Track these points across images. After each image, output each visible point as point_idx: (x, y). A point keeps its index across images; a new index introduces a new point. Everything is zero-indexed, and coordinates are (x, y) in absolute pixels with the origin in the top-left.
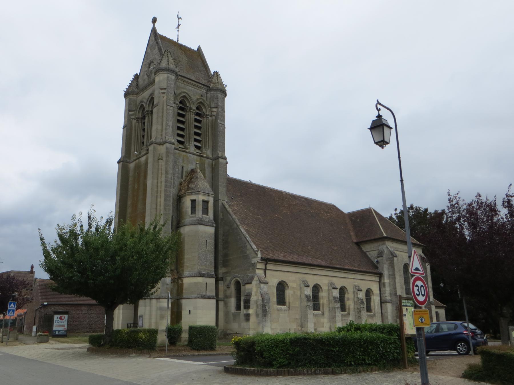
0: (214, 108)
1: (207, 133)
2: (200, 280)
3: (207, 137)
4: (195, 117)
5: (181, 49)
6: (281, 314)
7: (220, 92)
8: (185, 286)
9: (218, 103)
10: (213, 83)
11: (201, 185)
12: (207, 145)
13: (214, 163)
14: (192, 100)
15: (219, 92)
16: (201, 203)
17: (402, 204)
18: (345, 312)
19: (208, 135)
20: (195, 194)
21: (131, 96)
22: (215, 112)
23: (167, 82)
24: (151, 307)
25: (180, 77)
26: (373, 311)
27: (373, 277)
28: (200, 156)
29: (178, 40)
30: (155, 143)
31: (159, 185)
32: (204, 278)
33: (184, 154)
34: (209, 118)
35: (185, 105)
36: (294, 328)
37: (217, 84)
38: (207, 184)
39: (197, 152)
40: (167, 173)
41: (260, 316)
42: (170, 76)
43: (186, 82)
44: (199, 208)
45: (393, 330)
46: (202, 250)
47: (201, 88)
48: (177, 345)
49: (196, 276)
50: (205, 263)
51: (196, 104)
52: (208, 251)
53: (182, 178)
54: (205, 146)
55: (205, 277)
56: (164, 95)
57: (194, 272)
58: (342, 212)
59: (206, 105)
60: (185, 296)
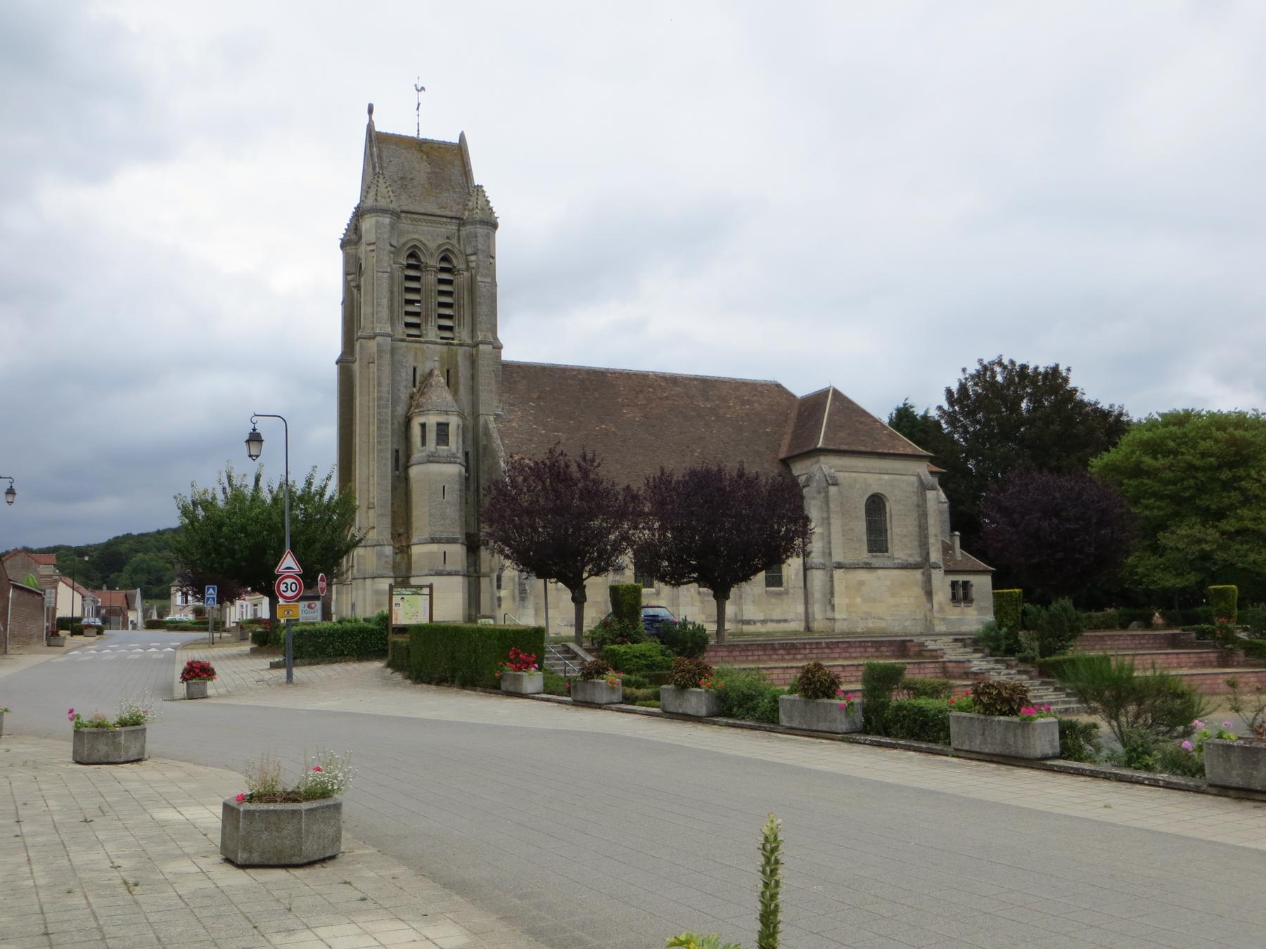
0: (472, 255)
1: (462, 302)
2: (434, 547)
3: (462, 310)
4: (439, 277)
5: (422, 151)
7: (480, 224)
8: (414, 558)
9: (477, 245)
10: (469, 210)
11: (434, 398)
13: (474, 352)
14: (427, 250)
15: (478, 226)
16: (434, 428)
17: (135, 533)
18: (780, 588)
19: (462, 306)
20: (424, 414)
21: (348, 248)
22: (474, 261)
23: (376, 231)
24: (364, 589)
25: (403, 215)
26: (785, 584)
28: (447, 344)
29: (418, 134)
30: (361, 338)
31: (371, 404)
33: (417, 345)
34: (463, 274)
35: (418, 259)
36: (592, 618)
37: (475, 212)
38: (447, 395)
39: (442, 338)
40: (379, 384)
41: (517, 599)
42: (381, 219)
43: (415, 220)
44: (432, 435)
47: (446, 225)
48: (104, 633)
49: (427, 543)
50: (442, 521)
51: (437, 255)
52: (448, 502)
53: (414, 386)
54: (459, 325)
55: (442, 543)
56: (374, 254)
57: (424, 537)
58: (794, 396)
59: (456, 251)
60: (413, 573)
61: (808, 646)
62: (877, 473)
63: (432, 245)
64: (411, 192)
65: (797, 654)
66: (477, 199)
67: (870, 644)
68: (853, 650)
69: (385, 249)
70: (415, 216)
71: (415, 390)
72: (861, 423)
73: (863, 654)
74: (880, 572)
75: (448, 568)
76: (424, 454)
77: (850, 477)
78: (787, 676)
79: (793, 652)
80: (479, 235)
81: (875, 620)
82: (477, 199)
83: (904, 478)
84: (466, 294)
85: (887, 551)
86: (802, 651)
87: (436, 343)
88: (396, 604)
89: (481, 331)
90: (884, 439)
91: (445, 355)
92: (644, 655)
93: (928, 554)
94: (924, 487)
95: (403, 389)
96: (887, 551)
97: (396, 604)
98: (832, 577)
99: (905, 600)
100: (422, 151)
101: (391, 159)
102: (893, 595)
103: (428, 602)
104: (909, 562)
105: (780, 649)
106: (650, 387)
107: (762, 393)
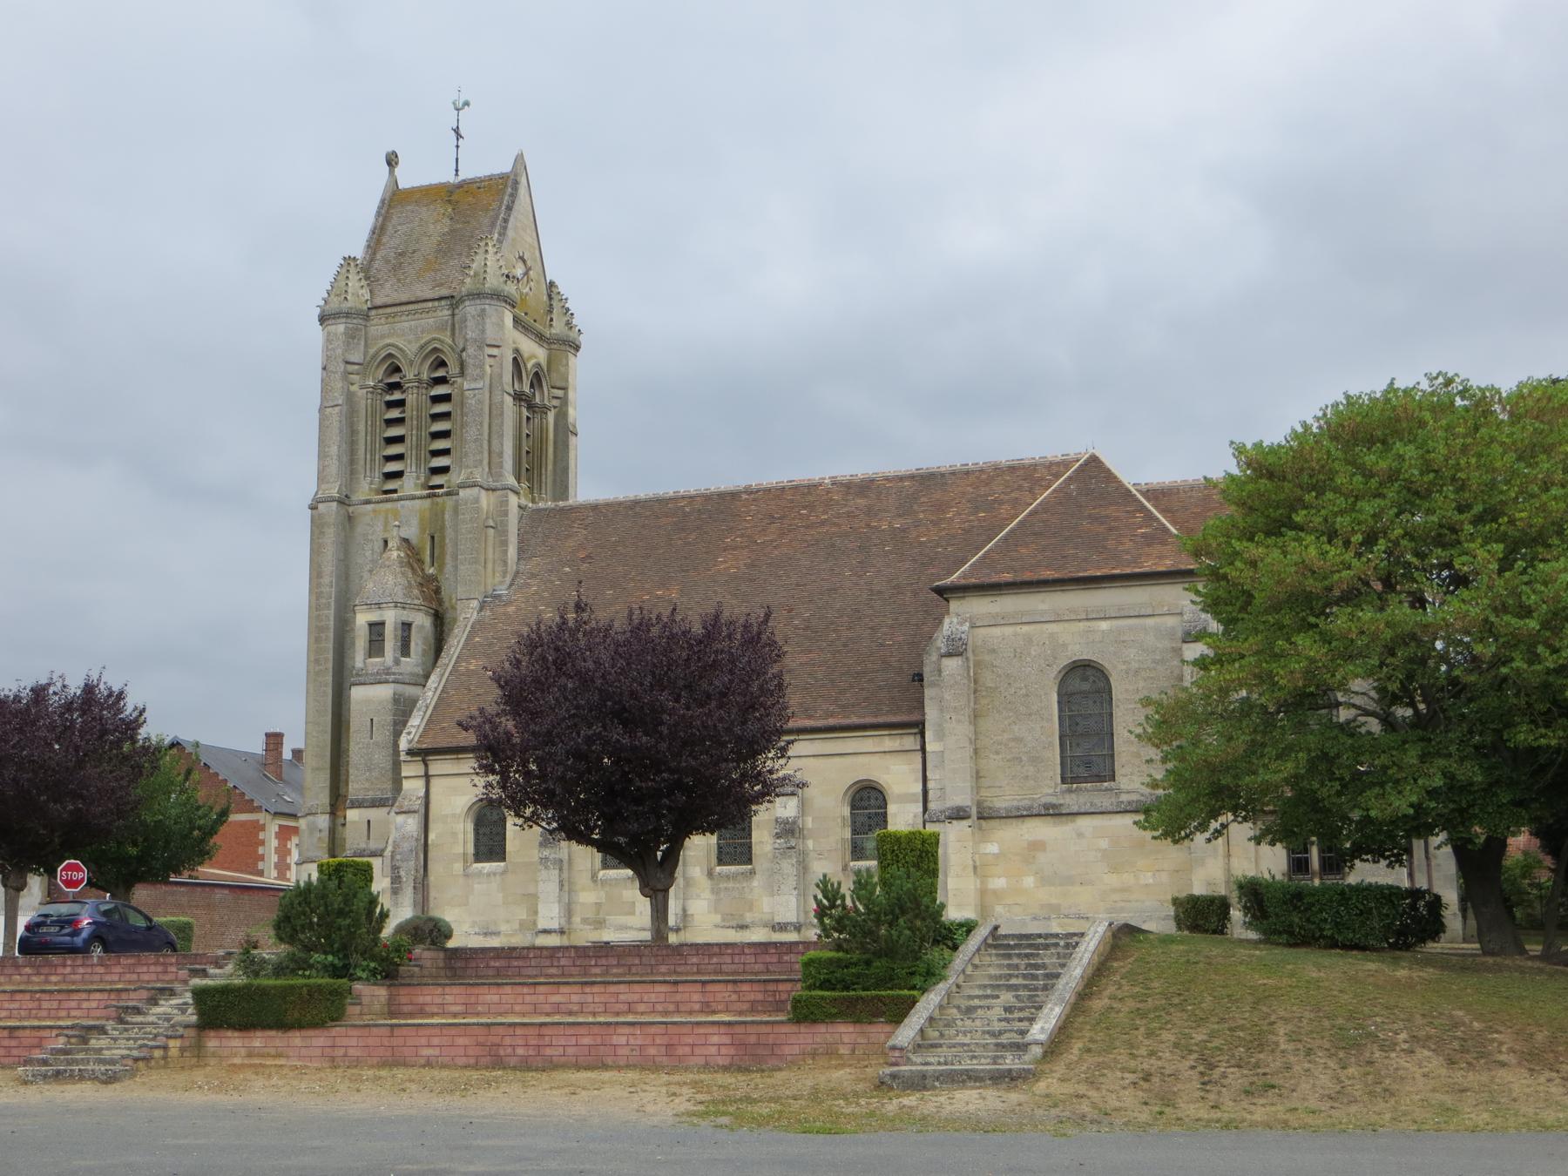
4: (433, 393)
6: (476, 886)
25: (373, 312)
27: (887, 738)
32: (363, 810)
33: (389, 505)
46: (361, 746)
52: (377, 744)
62: (1080, 620)
65: (51, 974)
68: (145, 969)
69: (337, 372)
70: (389, 310)
73: (161, 977)
74: (1084, 823)
77: (1015, 635)
81: (1066, 920)
83: (1150, 622)
86: (60, 970)
87: (413, 498)
91: (427, 514)
99: (1148, 878)
102: (1114, 869)
105: (25, 966)
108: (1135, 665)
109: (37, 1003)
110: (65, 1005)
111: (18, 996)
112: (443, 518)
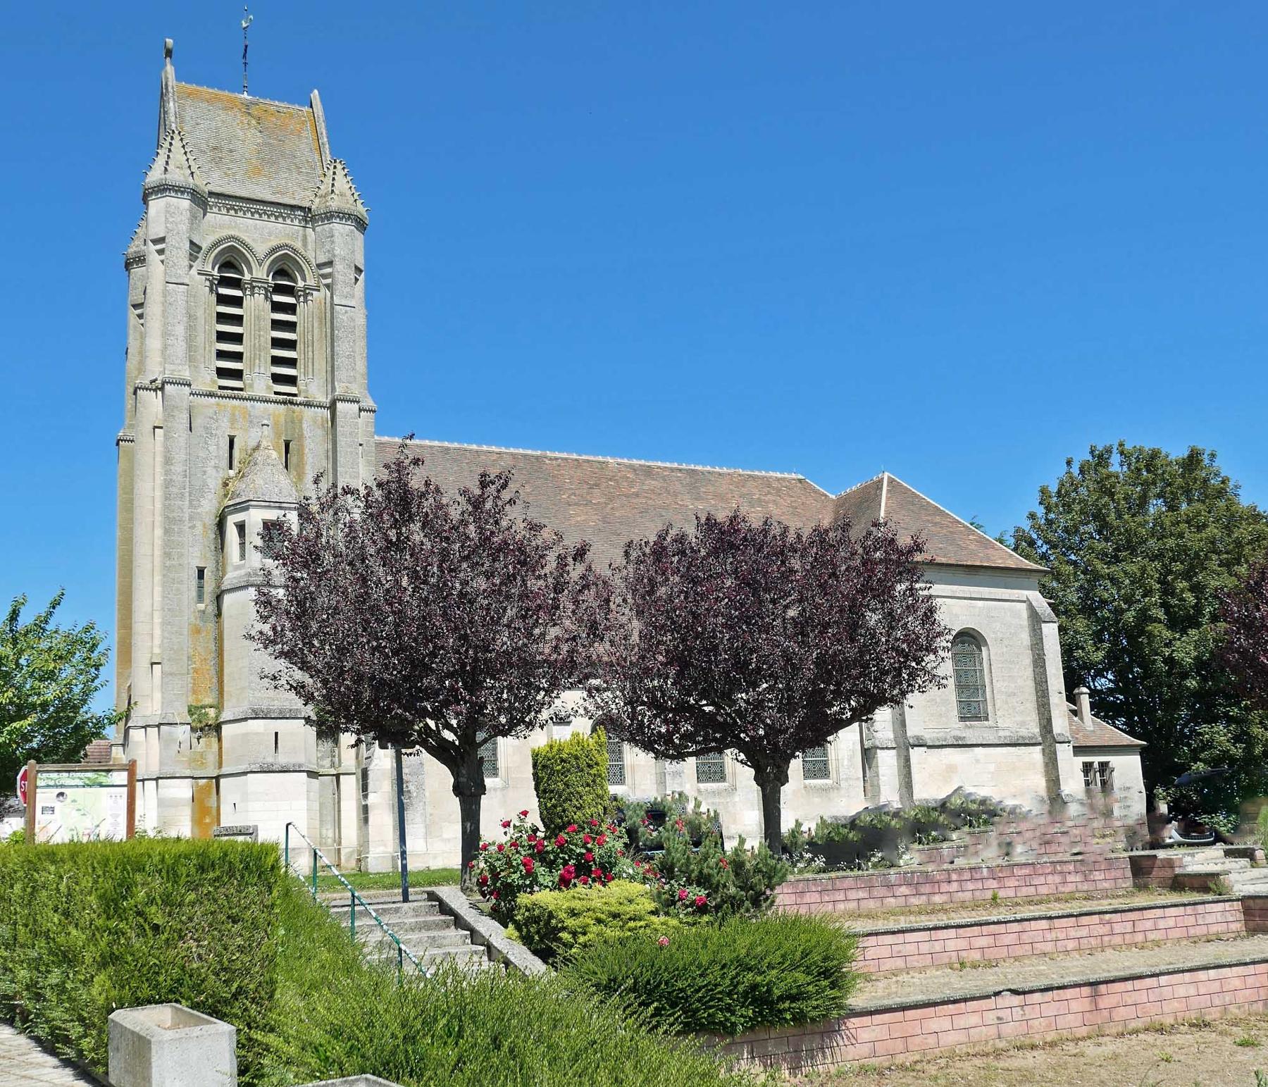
9: (333, 249)
12: (310, 370)
26: (833, 774)
33: (235, 402)
39: (276, 393)
45: (101, 1031)
61: (954, 877)
63: (261, 249)
64: (229, 169)
66: (334, 179)
67: (1071, 867)
68: (1042, 880)
71: (232, 473)
72: (935, 524)
75: (283, 759)
76: (243, 572)
78: (938, 947)
79: (926, 889)
80: (336, 234)
82: (334, 179)
84: (316, 325)
85: (987, 719)
86: (945, 887)
88: (44, 809)
89: (340, 381)
90: (973, 547)
91: (282, 419)
92: (615, 916)
93: (1049, 720)
94: (1036, 619)
95: (211, 471)
96: (987, 719)
97: (44, 809)
98: (907, 760)
100: (249, 114)
101: (199, 121)
103: (123, 802)
104: (1021, 734)
106: (610, 480)
107: (779, 490)
108: (1000, 635)
109: (1108, 926)
110: (1140, 926)
111: (1085, 920)
112: (301, 427)
